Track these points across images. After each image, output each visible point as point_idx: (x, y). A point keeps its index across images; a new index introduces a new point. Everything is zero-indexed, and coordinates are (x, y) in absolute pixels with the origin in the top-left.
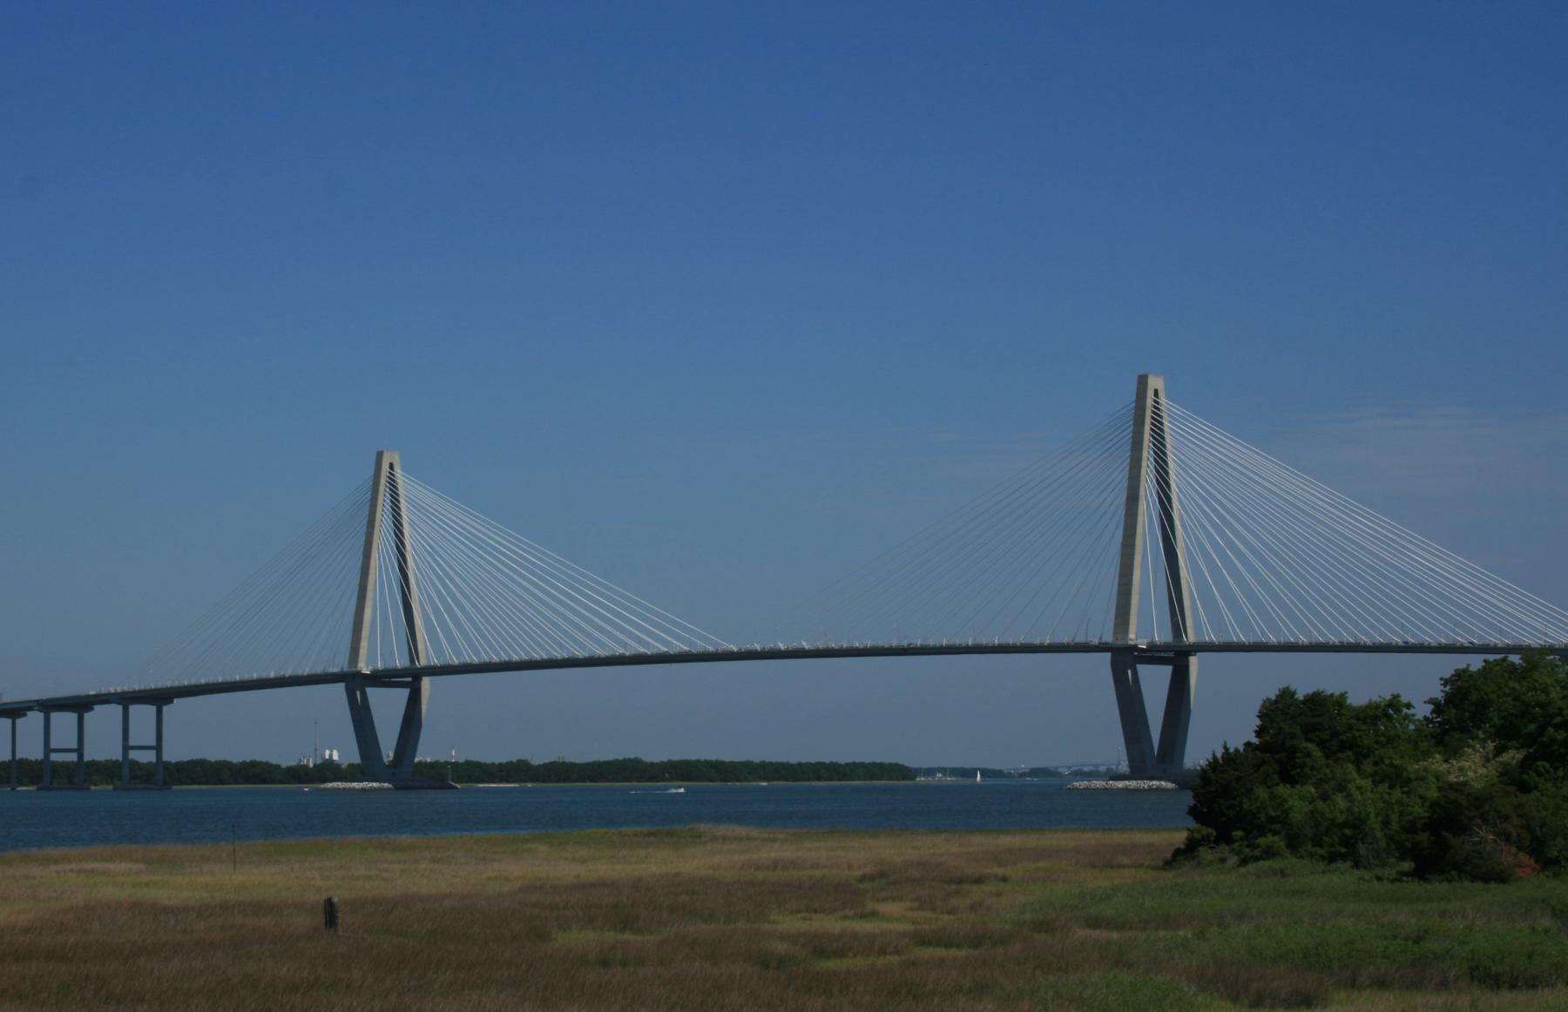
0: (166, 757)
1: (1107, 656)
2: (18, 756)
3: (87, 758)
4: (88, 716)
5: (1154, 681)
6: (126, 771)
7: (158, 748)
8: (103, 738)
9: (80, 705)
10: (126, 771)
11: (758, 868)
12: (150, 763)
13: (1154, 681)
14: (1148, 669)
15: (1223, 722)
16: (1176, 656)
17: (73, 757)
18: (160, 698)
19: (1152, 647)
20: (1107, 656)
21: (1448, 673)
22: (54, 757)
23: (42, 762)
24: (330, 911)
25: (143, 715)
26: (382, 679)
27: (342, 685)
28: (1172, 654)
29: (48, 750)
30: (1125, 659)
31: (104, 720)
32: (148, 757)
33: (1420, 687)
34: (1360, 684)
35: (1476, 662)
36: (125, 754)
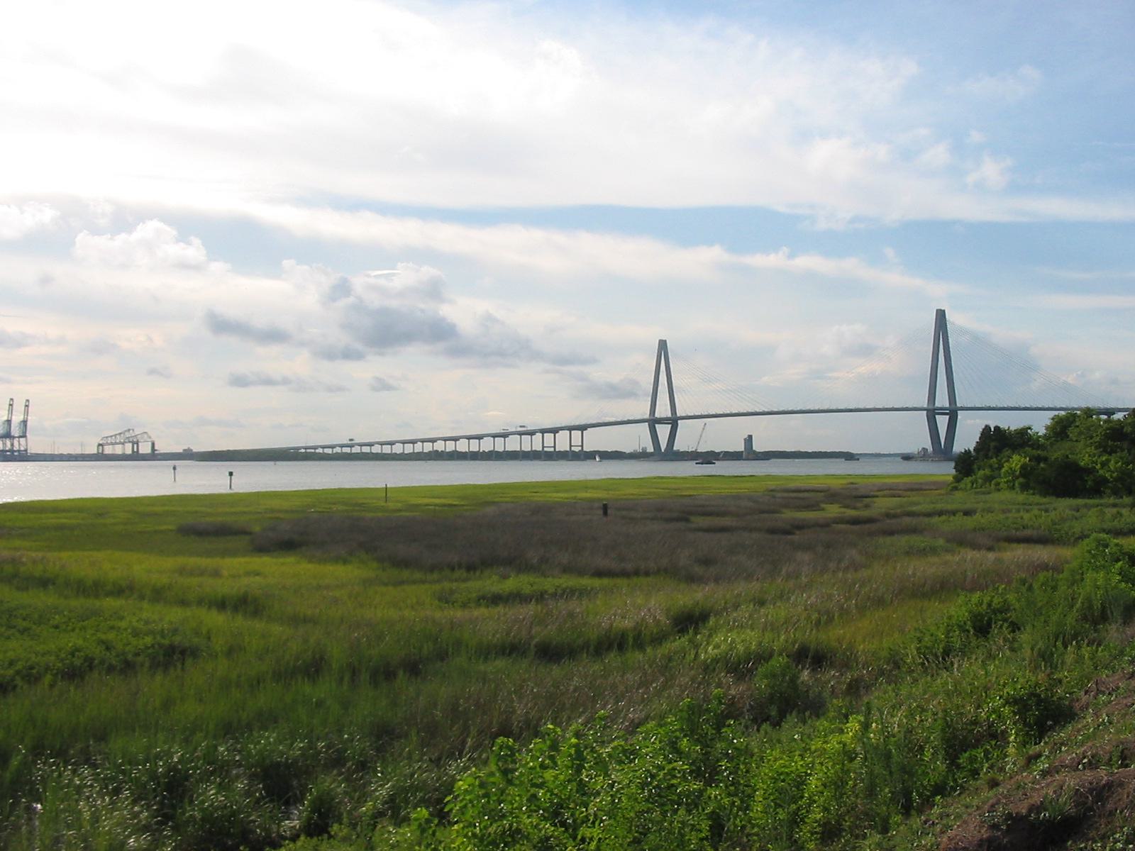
0: (585, 450)
1: (925, 412)
2: (533, 449)
3: (557, 450)
4: (557, 435)
5: (942, 421)
6: (570, 454)
7: (555, 447)
8: (320, 450)
9: (554, 431)
10: (570, 454)
11: (640, 495)
12: (539, 451)
13: (942, 421)
14: (942, 414)
15: (967, 438)
16: (953, 414)
17: (552, 449)
18: (582, 428)
19: (941, 409)
20: (925, 412)
21: (1052, 416)
22: (545, 449)
23: (402, 453)
24: (605, 508)
25: (576, 434)
26: (942, 411)
27: (647, 423)
28: (948, 411)
29: (543, 447)
30: (932, 413)
31: (563, 435)
32: (577, 449)
33: (1040, 424)
34: (1011, 422)
35: (1063, 413)
36: (570, 448)
